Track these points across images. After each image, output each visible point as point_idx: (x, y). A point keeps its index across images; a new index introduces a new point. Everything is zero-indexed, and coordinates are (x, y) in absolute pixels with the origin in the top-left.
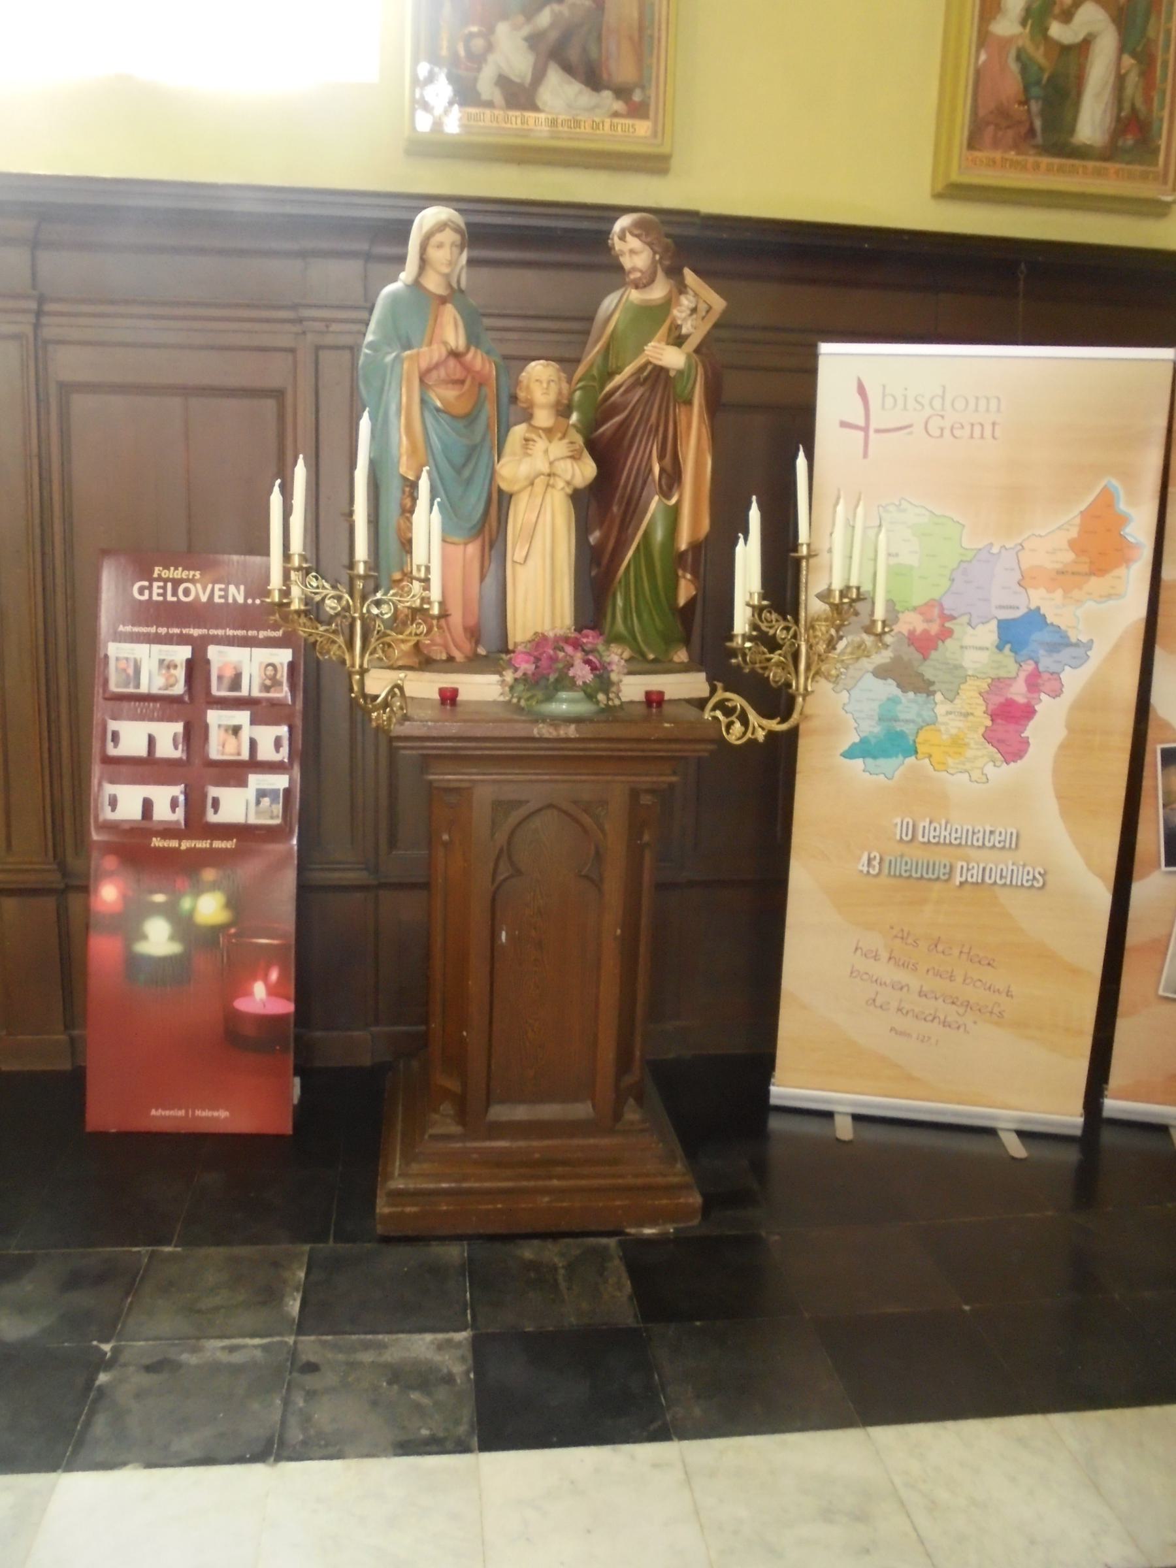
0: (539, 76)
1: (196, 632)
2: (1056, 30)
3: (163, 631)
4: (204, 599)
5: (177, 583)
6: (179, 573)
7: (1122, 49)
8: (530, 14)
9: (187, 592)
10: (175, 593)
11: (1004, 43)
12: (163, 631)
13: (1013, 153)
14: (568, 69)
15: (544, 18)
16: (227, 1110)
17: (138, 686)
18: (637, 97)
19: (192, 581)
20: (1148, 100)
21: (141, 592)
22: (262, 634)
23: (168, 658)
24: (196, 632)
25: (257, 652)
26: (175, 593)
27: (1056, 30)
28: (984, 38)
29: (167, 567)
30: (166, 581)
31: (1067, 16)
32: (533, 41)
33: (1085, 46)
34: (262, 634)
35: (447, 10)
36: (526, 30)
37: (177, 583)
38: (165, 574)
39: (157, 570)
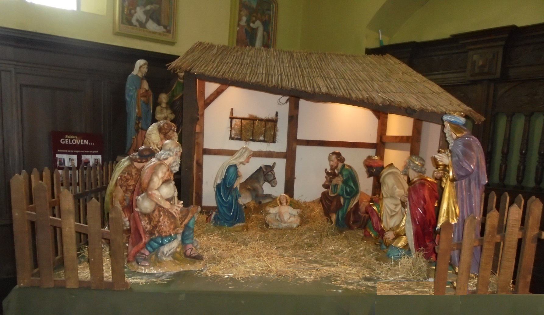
0: (147, 21)
1: (77, 152)
2: (252, 25)
3: (69, 151)
4: (79, 143)
5: (71, 139)
6: (72, 137)
7: (264, 31)
8: (145, 6)
9: (74, 142)
10: (71, 142)
11: (243, 27)
12: (69, 151)
13: (403, 243)
14: (152, 19)
15: (148, 7)
16: (127, 284)
17: (64, 165)
18: (168, 28)
19: (75, 139)
20: (269, 41)
21: (63, 141)
22: (93, 152)
23: (71, 158)
24: (77, 152)
25: (93, 156)
26: (71, 142)
27: (252, 25)
28: (239, 25)
29: (69, 135)
30: (69, 139)
31: (254, 23)
32: (146, 13)
33: (257, 29)
34: (93, 152)
35: (127, 3)
36: (144, 9)
37: (71, 139)
38: (68, 137)
39: (66, 136)
